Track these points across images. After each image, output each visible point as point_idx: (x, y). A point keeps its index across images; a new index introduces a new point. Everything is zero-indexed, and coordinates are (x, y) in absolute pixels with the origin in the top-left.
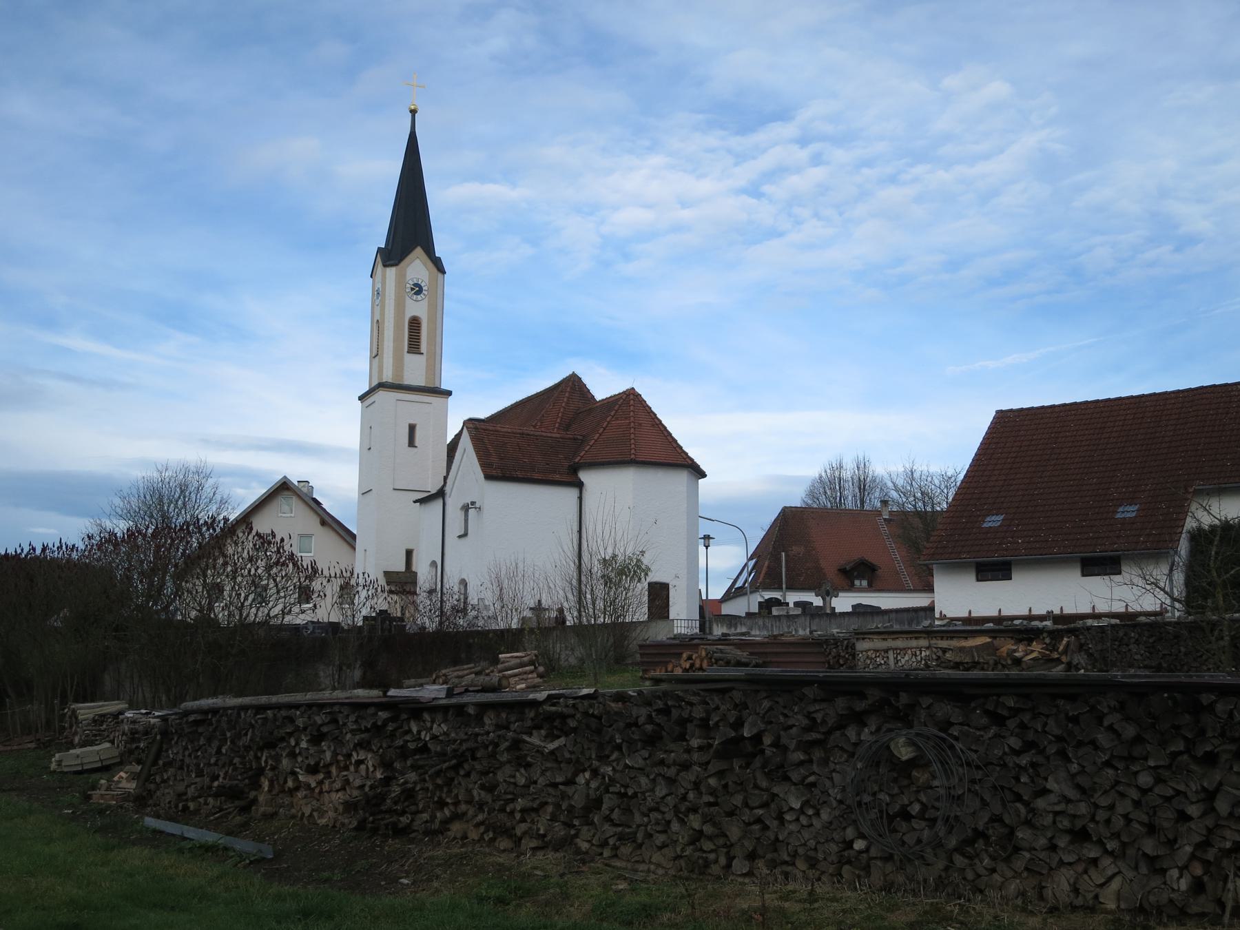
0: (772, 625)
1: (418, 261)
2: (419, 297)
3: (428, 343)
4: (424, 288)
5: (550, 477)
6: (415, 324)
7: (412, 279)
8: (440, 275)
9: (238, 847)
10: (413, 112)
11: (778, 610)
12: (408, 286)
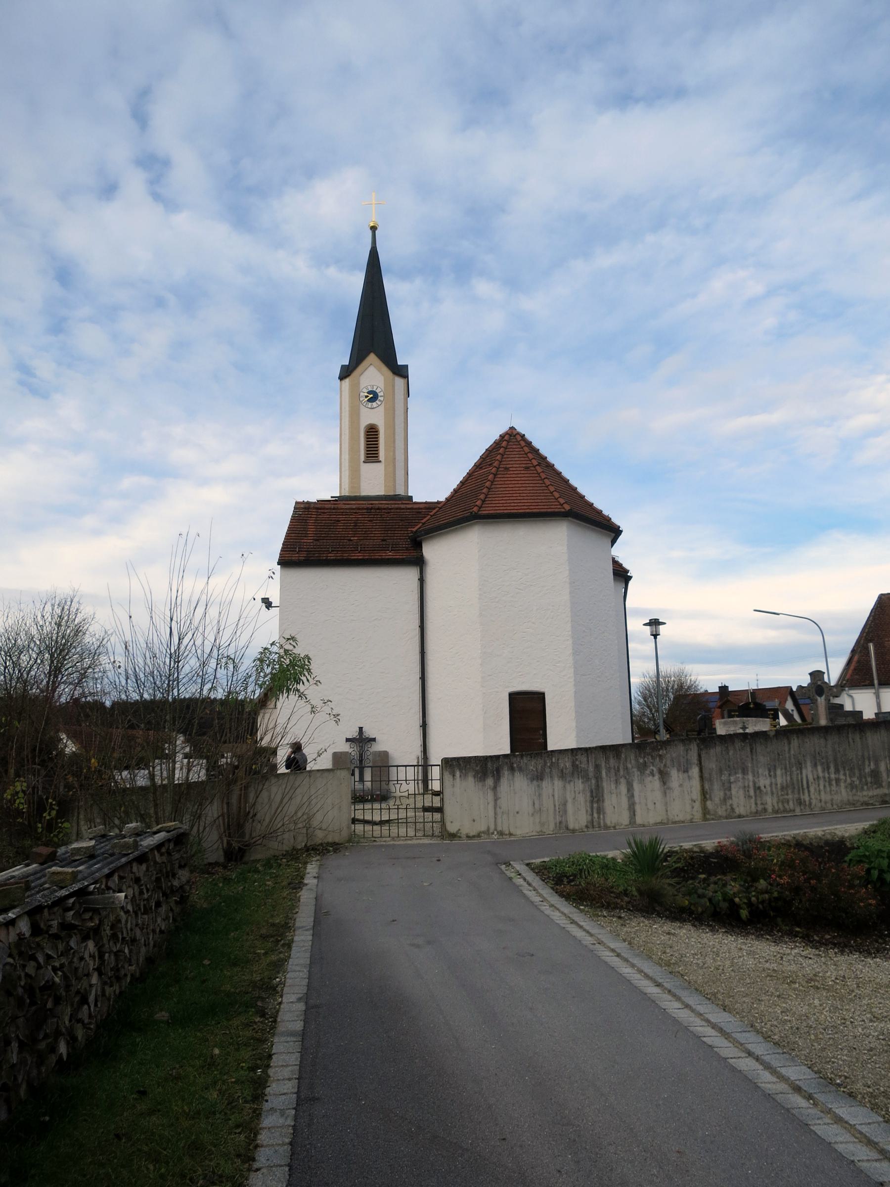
0: (597, 767)
1: (372, 369)
2: (374, 404)
3: (385, 450)
4: (379, 394)
5: (377, 556)
6: (372, 433)
7: (366, 387)
8: (399, 382)
9: (14, 1055)
10: (374, 229)
11: (725, 724)
12: (362, 394)
